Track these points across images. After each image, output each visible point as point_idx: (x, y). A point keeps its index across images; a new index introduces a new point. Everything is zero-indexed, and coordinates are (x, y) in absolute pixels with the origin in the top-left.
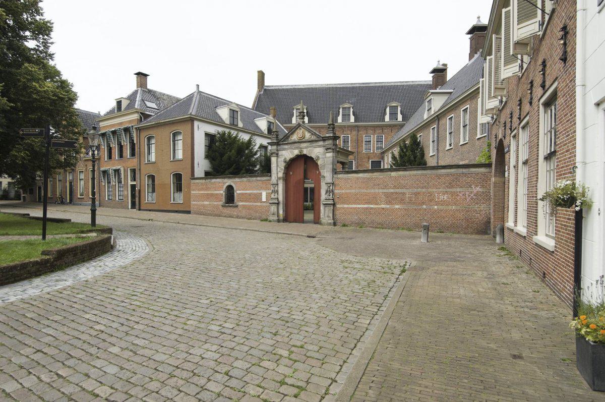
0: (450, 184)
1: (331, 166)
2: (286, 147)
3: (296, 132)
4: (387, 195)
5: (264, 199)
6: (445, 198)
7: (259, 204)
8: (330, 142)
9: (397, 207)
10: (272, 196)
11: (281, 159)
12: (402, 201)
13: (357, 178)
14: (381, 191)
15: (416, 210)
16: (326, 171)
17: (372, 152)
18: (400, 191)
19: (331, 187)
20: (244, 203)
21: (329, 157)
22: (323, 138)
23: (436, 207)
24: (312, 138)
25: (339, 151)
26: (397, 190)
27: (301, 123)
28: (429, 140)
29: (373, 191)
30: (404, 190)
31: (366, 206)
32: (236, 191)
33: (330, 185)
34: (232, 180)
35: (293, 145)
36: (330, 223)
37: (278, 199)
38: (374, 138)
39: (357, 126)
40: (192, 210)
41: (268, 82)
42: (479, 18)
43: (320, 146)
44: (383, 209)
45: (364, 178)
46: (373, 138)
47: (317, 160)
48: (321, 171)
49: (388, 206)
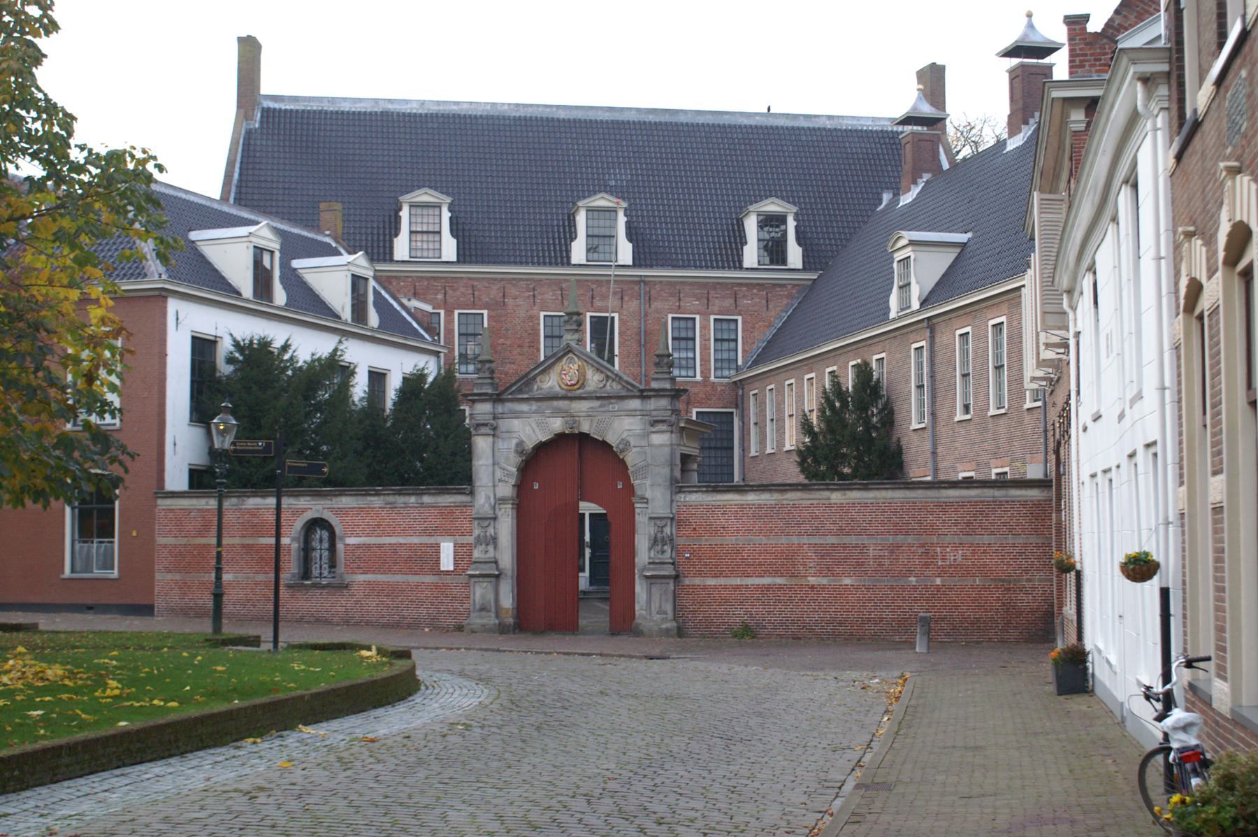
0: (969, 523)
1: (667, 471)
2: (524, 407)
3: (557, 368)
4: (824, 552)
5: (447, 563)
6: (959, 558)
7: (429, 579)
8: (664, 403)
9: (847, 581)
10: (477, 554)
11: (507, 448)
12: (859, 567)
13: (742, 507)
14: (805, 540)
15: (892, 588)
16: (652, 485)
17: (699, 378)
18: (852, 540)
19: (667, 530)
20: (369, 577)
21: (661, 446)
22: (642, 391)
23: (938, 581)
24: (608, 387)
25: (683, 428)
26: (847, 540)
27: (573, 344)
28: (908, 381)
29: (784, 540)
30: (864, 540)
31: (766, 581)
32: (342, 539)
33: (663, 523)
34: (326, 503)
35: (546, 404)
36: (667, 630)
37: (496, 562)
38: (705, 327)
39: (642, 281)
40: (159, 602)
41: (273, 83)
42: (1029, 15)
43: (631, 413)
44: (813, 587)
45: (760, 507)
46: (705, 328)
47: (622, 451)
48: (636, 483)
49: (824, 581)
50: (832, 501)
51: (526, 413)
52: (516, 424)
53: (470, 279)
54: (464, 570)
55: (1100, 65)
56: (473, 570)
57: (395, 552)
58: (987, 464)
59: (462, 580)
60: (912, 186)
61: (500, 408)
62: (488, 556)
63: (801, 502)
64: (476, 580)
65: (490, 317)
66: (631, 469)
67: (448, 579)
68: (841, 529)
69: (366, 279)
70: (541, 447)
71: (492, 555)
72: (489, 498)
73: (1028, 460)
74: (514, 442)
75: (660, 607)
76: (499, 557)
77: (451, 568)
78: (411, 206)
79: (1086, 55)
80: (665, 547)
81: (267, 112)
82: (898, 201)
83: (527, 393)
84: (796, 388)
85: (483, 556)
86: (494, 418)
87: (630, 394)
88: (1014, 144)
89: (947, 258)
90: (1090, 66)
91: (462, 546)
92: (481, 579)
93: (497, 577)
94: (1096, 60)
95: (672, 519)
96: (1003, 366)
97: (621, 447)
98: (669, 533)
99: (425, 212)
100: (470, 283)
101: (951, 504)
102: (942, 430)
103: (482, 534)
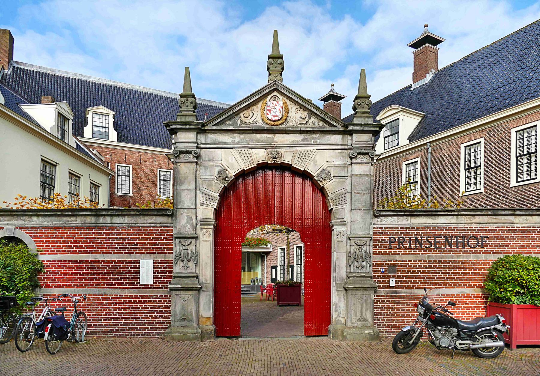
43: (331, 147)
50: (516, 225)
52: (219, 154)
53: (124, 150)
54: (163, 283)
56: (174, 284)
57: (92, 268)
59: (162, 292)
61: (202, 139)
62: (189, 270)
64: (178, 292)
65: (133, 168)
66: (330, 196)
69: (69, 120)
70: (242, 175)
71: (194, 271)
72: (191, 219)
74: (217, 169)
75: (362, 315)
76: (199, 272)
77: (151, 282)
78: (93, 113)
81: (16, 70)
85: (184, 271)
86: (197, 147)
87: (329, 128)
91: (162, 262)
92: (182, 292)
93: (199, 290)
96: (417, 182)
99: (101, 117)
100: (124, 152)
103: (183, 251)
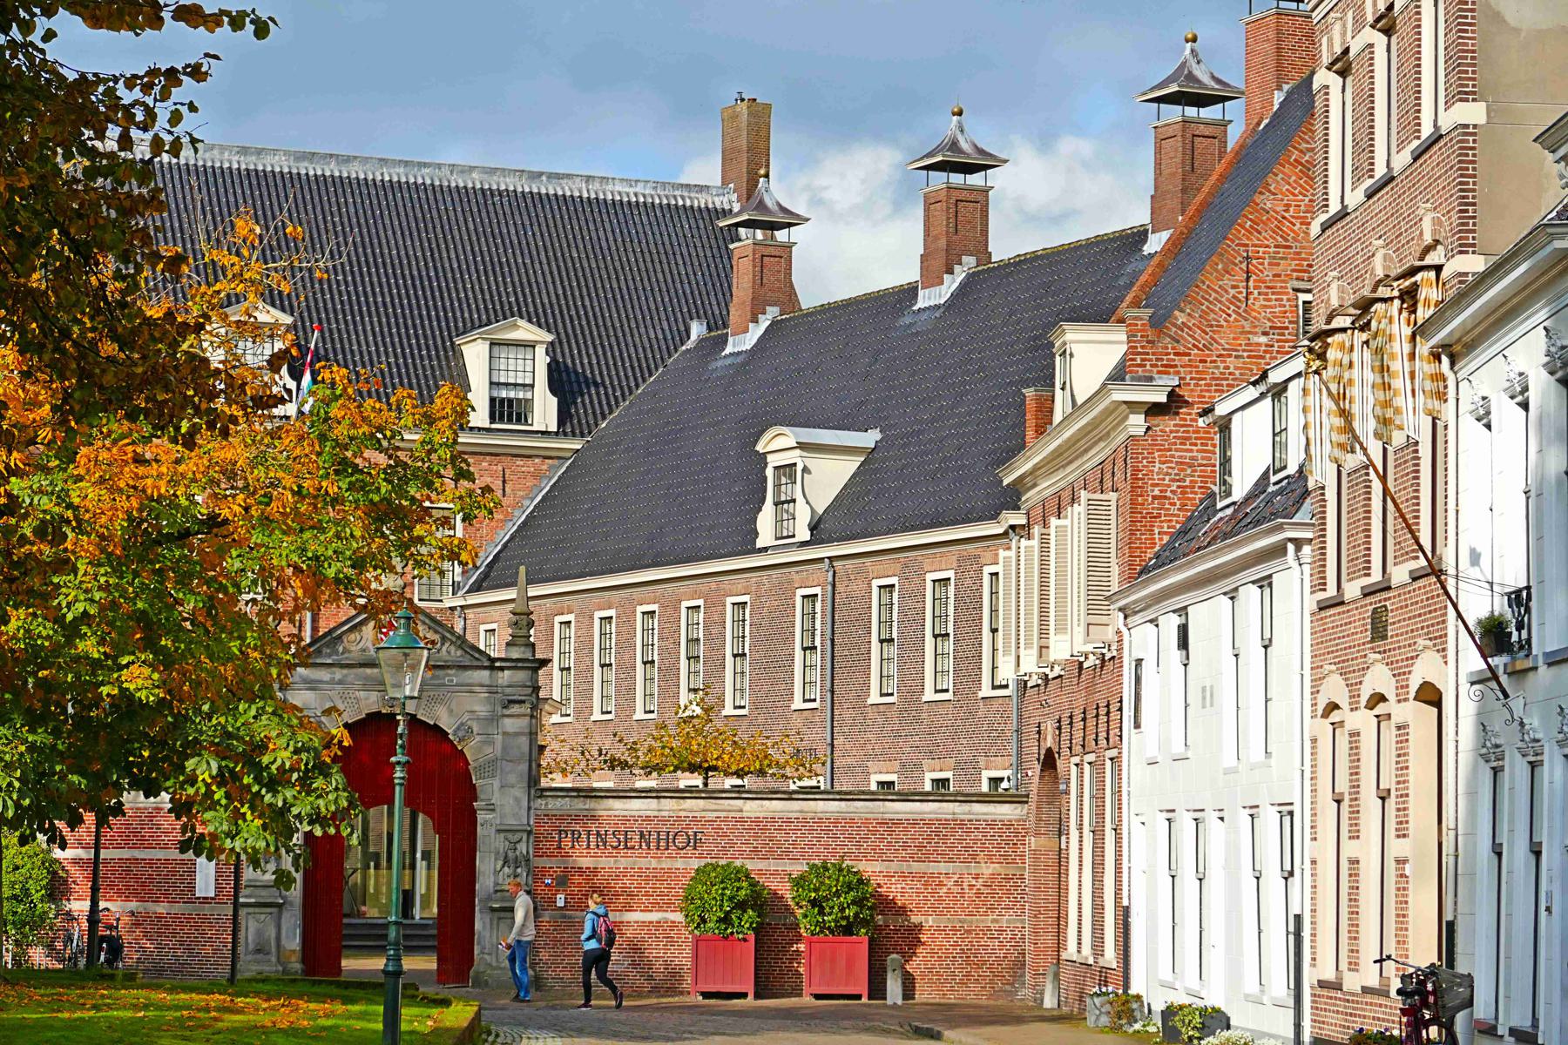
19: (522, 847)
21: (517, 734)
50: (745, 814)
51: (327, 683)
55: (1162, 366)
58: (918, 767)
60: (751, 325)
63: (703, 814)
64: (251, 910)
67: (207, 909)
68: (755, 850)
73: (982, 764)
79: (1148, 354)
80: (519, 870)
82: (723, 341)
83: (329, 656)
84: (578, 629)
87: (479, 664)
88: (929, 297)
89: (850, 466)
90: (1152, 366)
92: (257, 910)
94: (1157, 360)
95: (529, 833)
97: (460, 734)
98: (525, 852)
101: (898, 822)
102: (845, 714)
